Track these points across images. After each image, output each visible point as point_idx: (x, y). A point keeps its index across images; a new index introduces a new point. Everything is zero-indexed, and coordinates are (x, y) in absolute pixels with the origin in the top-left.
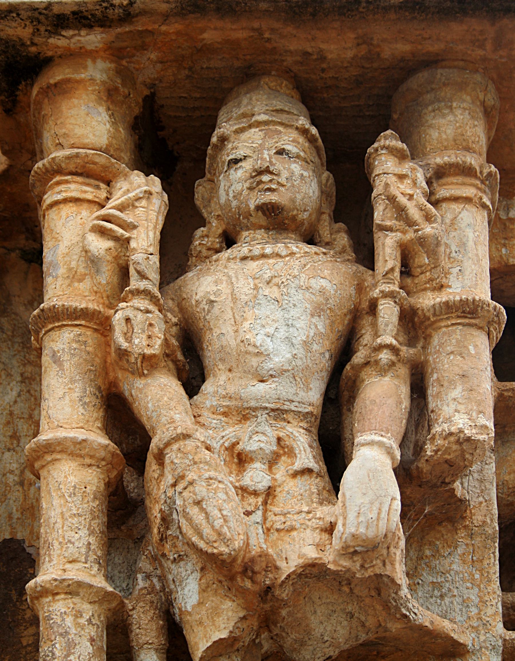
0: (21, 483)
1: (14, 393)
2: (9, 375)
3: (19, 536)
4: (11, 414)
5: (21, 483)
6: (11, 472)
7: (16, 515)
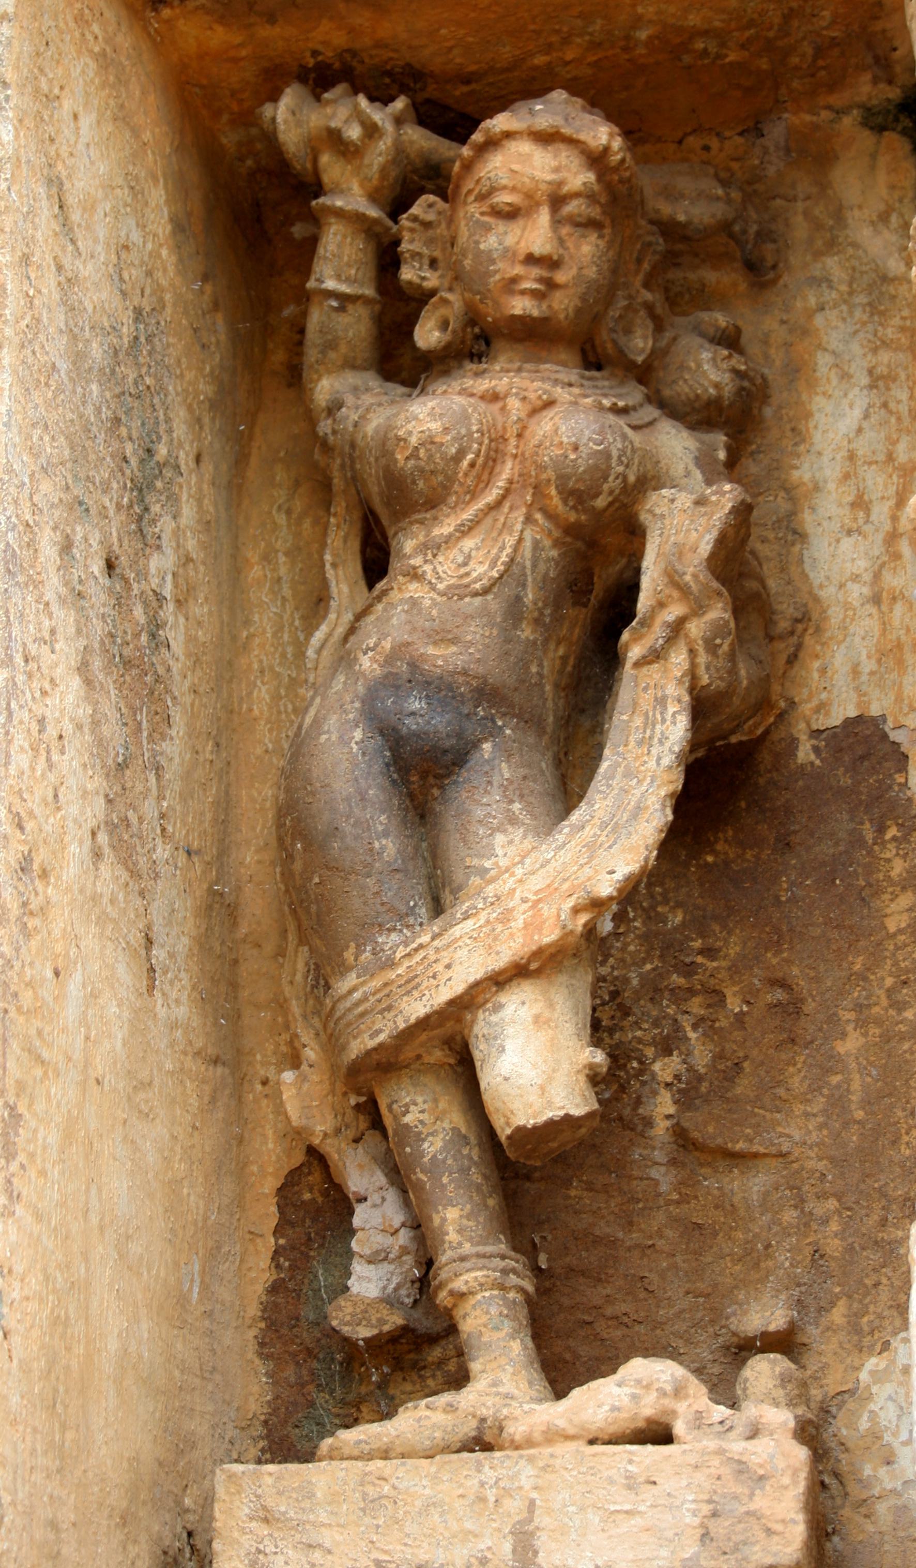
0: (876, 600)
1: (857, 413)
2: (845, 376)
3: (875, 710)
4: (851, 456)
5: (876, 600)
6: (856, 578)
7: (868, 666)
